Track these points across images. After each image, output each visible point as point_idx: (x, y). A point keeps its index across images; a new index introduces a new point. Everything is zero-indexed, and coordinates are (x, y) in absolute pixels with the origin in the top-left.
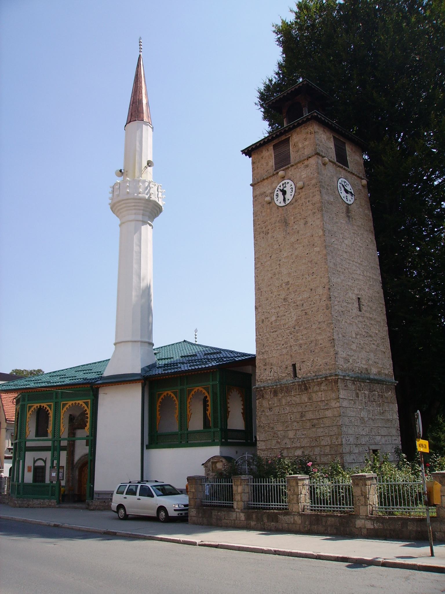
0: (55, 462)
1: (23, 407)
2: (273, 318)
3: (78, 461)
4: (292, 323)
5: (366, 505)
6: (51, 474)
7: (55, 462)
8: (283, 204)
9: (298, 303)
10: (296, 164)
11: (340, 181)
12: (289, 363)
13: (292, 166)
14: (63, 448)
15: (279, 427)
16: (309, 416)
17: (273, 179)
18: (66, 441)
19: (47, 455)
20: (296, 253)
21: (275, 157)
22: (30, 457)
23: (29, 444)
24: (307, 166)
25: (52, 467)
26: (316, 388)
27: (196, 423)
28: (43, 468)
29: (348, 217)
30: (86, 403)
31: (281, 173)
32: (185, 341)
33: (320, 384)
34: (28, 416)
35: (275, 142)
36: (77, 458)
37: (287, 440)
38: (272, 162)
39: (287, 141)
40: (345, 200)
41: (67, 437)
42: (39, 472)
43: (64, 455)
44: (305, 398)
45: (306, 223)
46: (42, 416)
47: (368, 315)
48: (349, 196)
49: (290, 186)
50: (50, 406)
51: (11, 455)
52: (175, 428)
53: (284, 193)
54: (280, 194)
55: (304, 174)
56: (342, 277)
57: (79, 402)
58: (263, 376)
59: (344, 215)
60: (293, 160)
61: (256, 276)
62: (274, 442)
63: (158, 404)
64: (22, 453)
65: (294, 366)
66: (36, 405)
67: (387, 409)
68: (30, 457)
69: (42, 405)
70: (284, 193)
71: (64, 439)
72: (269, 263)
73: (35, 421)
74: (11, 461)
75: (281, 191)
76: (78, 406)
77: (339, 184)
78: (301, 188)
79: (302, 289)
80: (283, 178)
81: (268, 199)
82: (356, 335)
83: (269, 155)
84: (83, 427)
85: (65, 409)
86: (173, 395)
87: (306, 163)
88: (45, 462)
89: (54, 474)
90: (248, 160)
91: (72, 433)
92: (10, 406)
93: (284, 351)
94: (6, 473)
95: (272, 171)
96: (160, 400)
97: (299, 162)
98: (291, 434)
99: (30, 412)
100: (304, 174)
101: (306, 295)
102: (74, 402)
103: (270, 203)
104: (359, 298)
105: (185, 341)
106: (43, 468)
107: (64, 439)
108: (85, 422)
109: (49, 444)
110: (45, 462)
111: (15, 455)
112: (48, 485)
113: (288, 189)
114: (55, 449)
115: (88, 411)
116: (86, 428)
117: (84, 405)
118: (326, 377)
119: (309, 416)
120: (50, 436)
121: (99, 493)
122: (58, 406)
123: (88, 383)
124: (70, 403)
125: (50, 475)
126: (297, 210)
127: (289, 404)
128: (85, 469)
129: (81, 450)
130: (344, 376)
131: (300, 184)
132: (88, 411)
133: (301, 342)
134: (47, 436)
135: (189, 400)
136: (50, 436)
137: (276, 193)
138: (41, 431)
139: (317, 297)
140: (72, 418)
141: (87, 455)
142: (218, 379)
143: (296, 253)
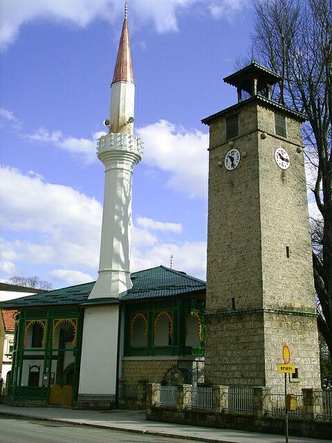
0: (47, 369)
1: (22, 323)
2: (220, 261)
3: (68, 367)
4: (233, 266)
5: (261, 409)
6: (43, 378)
7: (47, 369)
8: (230, 169)
9: (238, 250)
10: (242, 136)
11: (277, 151)
12: (230, 297)
13: (239, 138)
14: (54, 358)
15: (221, 347)
16: (242, 340)
17: (224, 146)
18: (57, 352)
19: (41, 363)
20: (239, 209)
21: (228, 128)
22: (26, 363)
23: (26, 353)
24: (250, 139)
25: (45, 373)
26: (248, 318)
27: (162, 340)
28: (37, 374)
29: (283, 180)
30: (74, 321)
31: (231, 143)
32: (161, 266)
33: (251, 315)
34: (26, 329)
35: (228, 115)
36: (66, 365)
37: (226, 358)
38: (224, 133)
39: (236, 116)
40: (281, 166)
41: (57, 348)
42: (34, 377)
43: (55, 362)
44: (240, 326)
45: (247, 186)
46: (37, 330)
47: (295, 260)
48: (285, 163)
49: (236, 154)
50: (44, 322)
51: (11, 361)
52: (145, 345)
53: (232, 159)
54: (229, 160)
55: (247, 146)
56: (273, 230)
57: (69, 319)
58: (212, 305)
59: (279, 179)
60: (240, 134)
61: (209, 226)
62: (217, 359)
63: (132, 324)
64: (20, 361)
65: (233, 299)
66: (32, 321)
67: (308, 336)
68: (26, 363)
69: (38, 321)
70: (232, 159)
71: (55, 350)
72: (218, 215)
73: (31, 334)
74: (118, 307)
75: (230, 157)
76: (66, 323)
77: (276, 153)
78: (245, 157)
79: (242, 239)
80: (232, 147)
81: (220, 163)
82: (283, 277)
83: (223, 125)
84: (71, 340)
85: (56, 325)
86: (143, 317)
87: (249, 136)
88: (39, 368)
89: (46, 378)
90: (207, 127)
91: (62, 345)
92: (10, 318)
93: (227, 288)
94: (4, 376)
95: (224, 140)
96: (134, 320)
97: (244, 135)
98: (229, 354)
99: (28, 327)
100: (247, 146)
101: (244, 245)
102: (64, 319)
103: (221, 166)
104: (287, 247)
105: (161, 266)
106: (37, 374)
107: (55, 350)
108: (72, 336)
109: (42, 353)
110: (39, 368)
111: (14, 360)
112: (40, 389)
113: (235, 157)
114: (48, 358)
115: (76, 328)
116: (73, 342)
117: (72, 322)
118: (255, 310)
119: (242, 340)
120: (43, 348)
121: (83, 396)
122: (50, 320)
123: (76, 304)
124: (61, 320)
125: (43, 379)
126: (241, 174)
127: (227, 329)
128: (71, 375)
129: (69, 359)
130: (269, 310)
131: (244, 153)
132: (76, 328)
133: (239, 281)
134: (41, 347)
135: (156, 322)
136: (43, 348)
137: (226, 158)
138: (36, 343)
139: (252, 246)
140: (62, 333)
141: (74, 363)
142: (179, 306)
143: (239, 209)
